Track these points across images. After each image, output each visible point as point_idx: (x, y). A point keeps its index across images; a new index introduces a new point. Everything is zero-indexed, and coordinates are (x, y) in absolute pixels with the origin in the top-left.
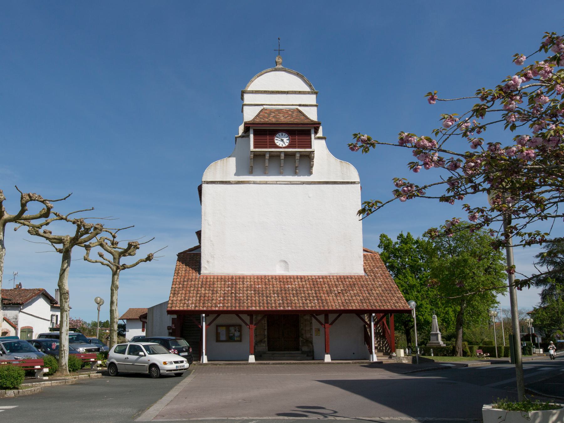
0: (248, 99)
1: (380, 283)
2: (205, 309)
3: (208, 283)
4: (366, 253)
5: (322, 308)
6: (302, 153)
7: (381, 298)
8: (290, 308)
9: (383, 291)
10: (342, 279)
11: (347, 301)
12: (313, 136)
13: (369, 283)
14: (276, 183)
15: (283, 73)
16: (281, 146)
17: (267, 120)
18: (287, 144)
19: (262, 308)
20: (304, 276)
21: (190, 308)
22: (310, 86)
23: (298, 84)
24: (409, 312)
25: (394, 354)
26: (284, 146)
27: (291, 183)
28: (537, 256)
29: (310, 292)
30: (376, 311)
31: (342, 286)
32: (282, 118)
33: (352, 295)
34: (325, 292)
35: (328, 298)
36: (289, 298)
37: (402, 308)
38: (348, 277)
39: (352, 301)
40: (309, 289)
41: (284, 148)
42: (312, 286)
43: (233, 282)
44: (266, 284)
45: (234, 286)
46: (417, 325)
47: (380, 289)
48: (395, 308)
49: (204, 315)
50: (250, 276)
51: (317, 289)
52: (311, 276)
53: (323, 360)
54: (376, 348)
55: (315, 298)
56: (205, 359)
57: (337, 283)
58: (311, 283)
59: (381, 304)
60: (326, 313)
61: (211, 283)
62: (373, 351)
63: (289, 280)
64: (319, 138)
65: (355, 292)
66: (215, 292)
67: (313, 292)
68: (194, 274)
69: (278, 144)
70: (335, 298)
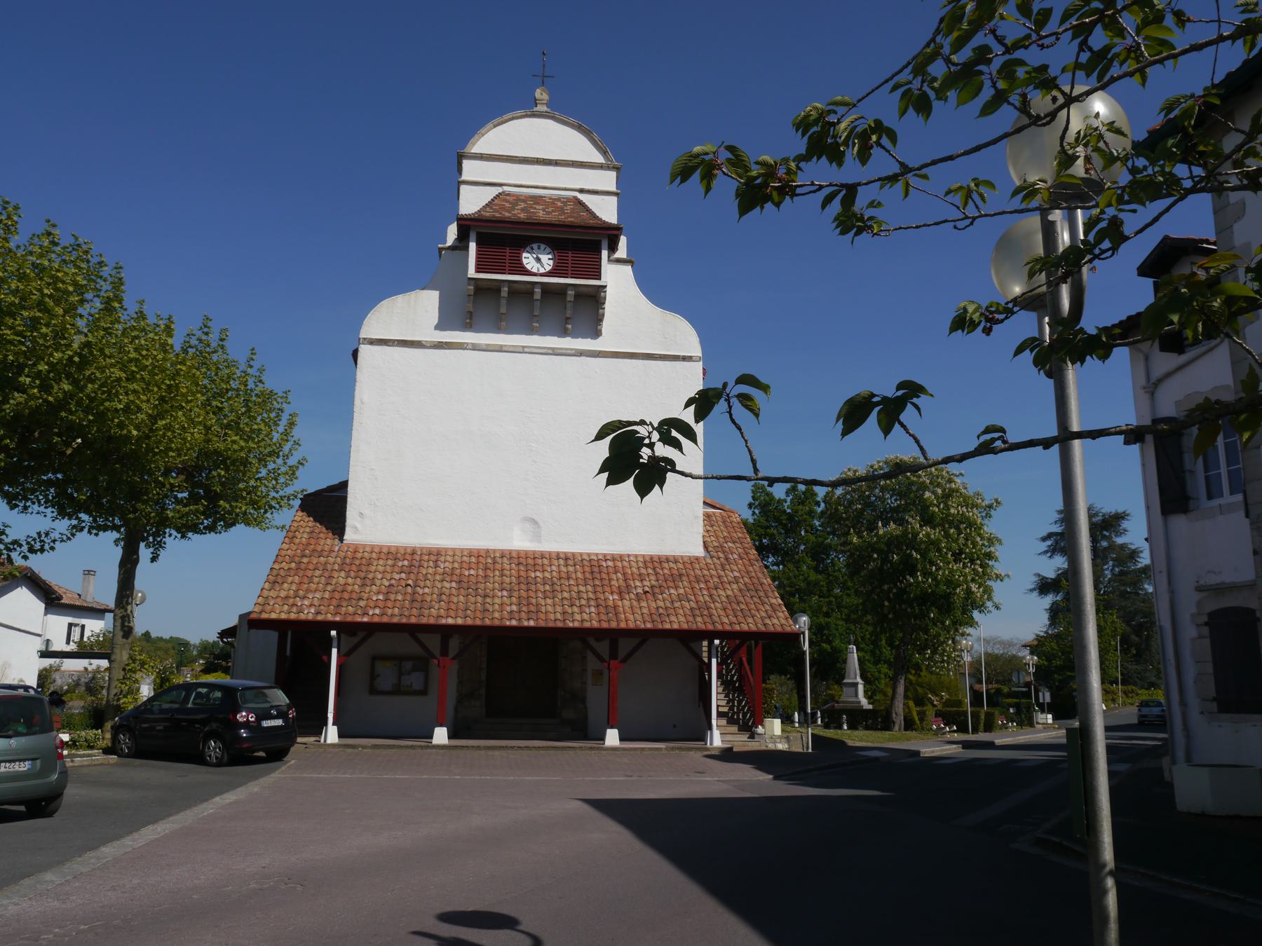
0: (471, 170)
1: (737, 574)
2: (338, 619)
3: (357, 562)
4: (711, 510)
5: (605, 625)
6: (582, 289)
7: (735, 606)
8: (532, 623)
9: (740, 590)
10: (655, 562)
11: (661, 611)
12: (605, 253)
13: (714, 573)
14: (522, 350)
15: (550, 122)
16: (535, 270)
17: (507, 214)
18: (548, 268)
19: (469, 622)
20: (573, 554)
21: (302, 617)
22: (604, 153)
23: (577, 145)
24: (795, 637)
25: (760, 729)
26: (542, 271)
27: (555, 352)
28: (1044, 539)
29: (582, 588)
30: (722, 635)
31: (653, 578)
32: (541, 213)
33: (674, 597)
34: (614, 589)
35: (620, 603)
36: (534, 601)
37: (779, 629)
38: (668, 559)
39: (672, 611)
40: (580, 582)
41: (542, 275)
42: (588, 575)
43: (413, 561)
44: (486, 569)
45: (415, 571)
46: (1103, 606)
47: (735, 586)
48: (763, 628)
49: (333, 633)
50: (454, 550)
51: (597, 582)
52: (589, 555)
53: (603, 738)
54: (720, 715)
55: (592, 603)
56: (332, 734)
57: (643, 571)
58: (587, 569)
59: (734, 620)
60: (613, 636)
61: (361, 562)
62: (714, 722)
63: (540, 562)
64: (619, 261)
65: (681, 591)
66: (368, 582)
67: (589, 588)
68: (328, 541)
69: (529, 267)
70: (635, 603)
